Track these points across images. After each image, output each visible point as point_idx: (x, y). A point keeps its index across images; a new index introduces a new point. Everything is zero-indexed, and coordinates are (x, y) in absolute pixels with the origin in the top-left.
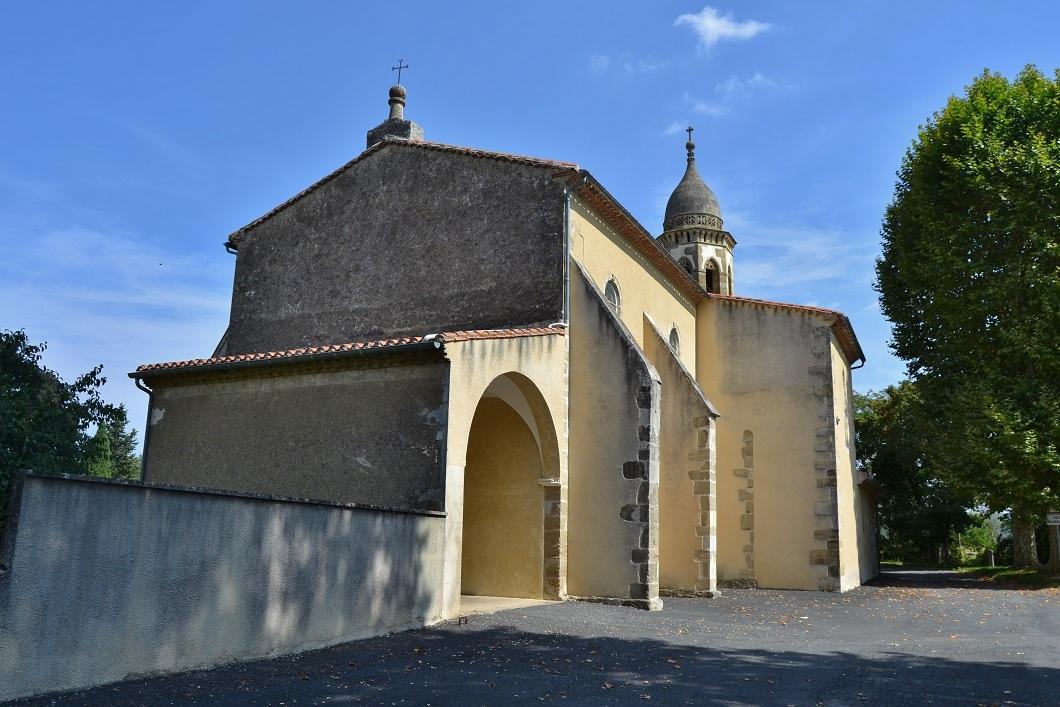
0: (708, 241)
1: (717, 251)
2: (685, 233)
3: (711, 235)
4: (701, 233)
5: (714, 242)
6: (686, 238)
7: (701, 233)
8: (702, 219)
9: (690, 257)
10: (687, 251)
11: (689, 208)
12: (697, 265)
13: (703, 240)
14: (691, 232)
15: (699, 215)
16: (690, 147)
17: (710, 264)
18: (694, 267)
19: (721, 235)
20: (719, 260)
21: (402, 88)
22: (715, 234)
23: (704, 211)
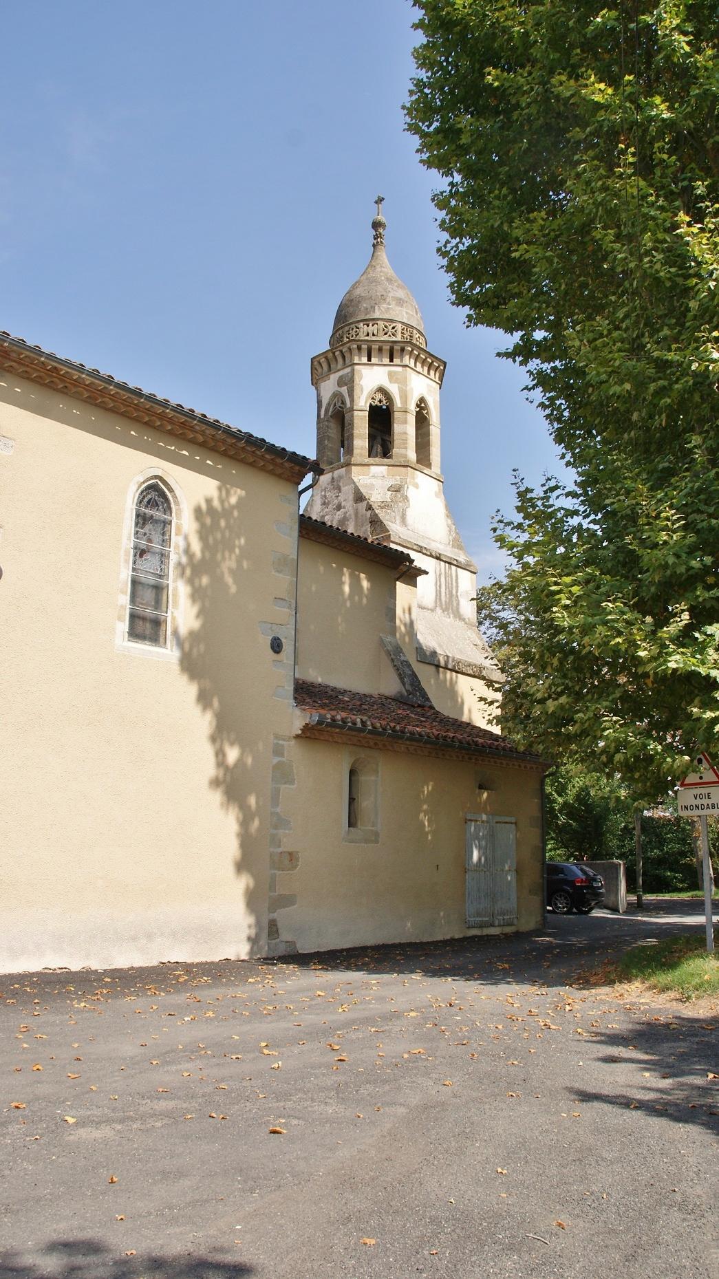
0: (374, 360)
1: (390, 374)
2: (364, 347)
3: (380, 350)
4: (359, 348)
5: (386, 361)
6: (340, 360)
7: (359, 348)
8: (371, 329)
9: (344, 390)
10: (341, 382)
11: (352, 316)
12: (352, 401)
13: (365, 360)
14: (375, 347)
15: (367, 322)
16: (376, 225)
17: (379, 396)
18: (348, 405)
19: (397, 347)
20: (394, 390)
21: (381, 218)
22: (386, 347)
23: (377, 315)
